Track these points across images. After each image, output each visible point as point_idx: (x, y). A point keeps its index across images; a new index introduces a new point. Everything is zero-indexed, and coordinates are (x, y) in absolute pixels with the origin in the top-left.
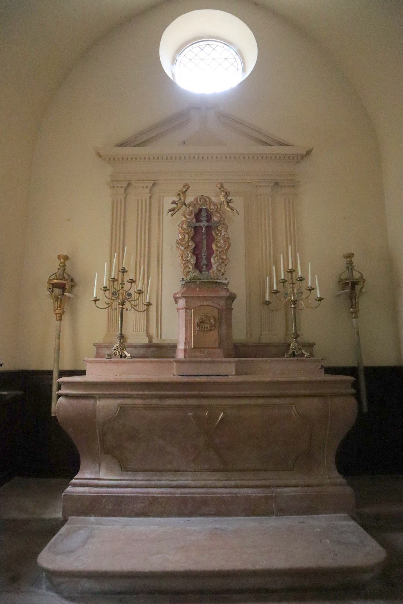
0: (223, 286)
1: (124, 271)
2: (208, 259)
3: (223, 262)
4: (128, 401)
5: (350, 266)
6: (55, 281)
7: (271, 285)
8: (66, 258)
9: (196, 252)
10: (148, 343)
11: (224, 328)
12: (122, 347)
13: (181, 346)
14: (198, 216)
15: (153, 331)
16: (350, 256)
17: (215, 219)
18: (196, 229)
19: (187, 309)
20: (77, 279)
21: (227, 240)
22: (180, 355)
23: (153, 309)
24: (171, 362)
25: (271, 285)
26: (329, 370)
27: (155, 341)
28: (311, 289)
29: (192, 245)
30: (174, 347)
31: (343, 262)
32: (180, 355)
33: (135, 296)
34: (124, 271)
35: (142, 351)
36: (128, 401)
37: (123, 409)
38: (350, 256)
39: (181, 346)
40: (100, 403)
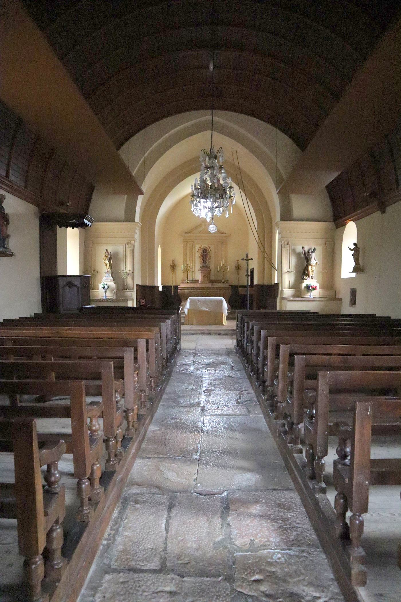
0: (208, 268)
1: (188, 264)
2: (206, 261)
3: (209, 262)
4: (191, 290)
5: (238, 263)
6: (362, 426)
7: (221, 265)
8: (174, 260)
9: (203, 259)
10: (139, 195)
11: (209, 277)
12: (188, 280)
13: (200, 280)
14: (204, 251)
15: (193, 277)
16: (238, 261)
17: (208, 252)
18: (203, 254)
19: (201, 273)
20: (176, 265)
21: (210, 256)
22: (200, 282)
23: (193, 273)
24: (171, 508)
25: (221, 265)
26: (230, 286)
27: (194, 279)
28: (227, 269)
29: (202, 258)
30: (198, 281)
31: (237, 262)
32: (200, 282)
33: (190, 270)
34: (188, 264)
35: (192, 281)
36: (191, 290)
37: (190, 292)
38: (238, 261)
39: (200, 280)
40: (186, 291)
